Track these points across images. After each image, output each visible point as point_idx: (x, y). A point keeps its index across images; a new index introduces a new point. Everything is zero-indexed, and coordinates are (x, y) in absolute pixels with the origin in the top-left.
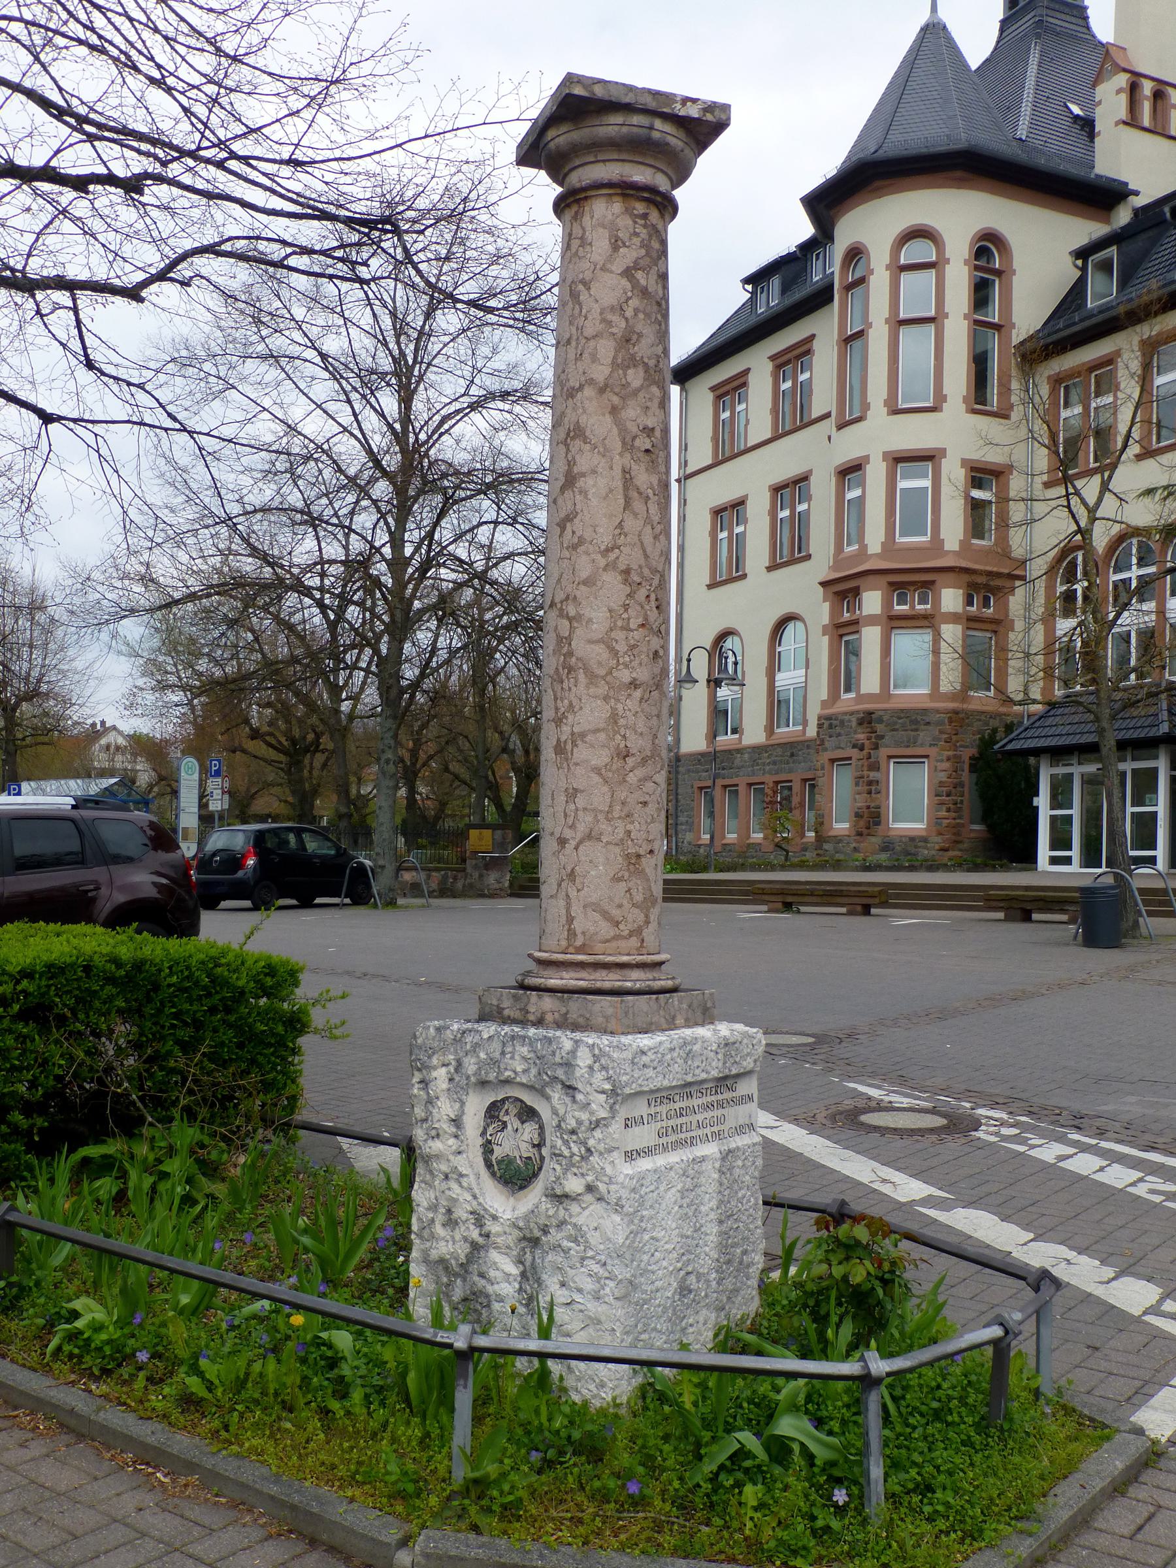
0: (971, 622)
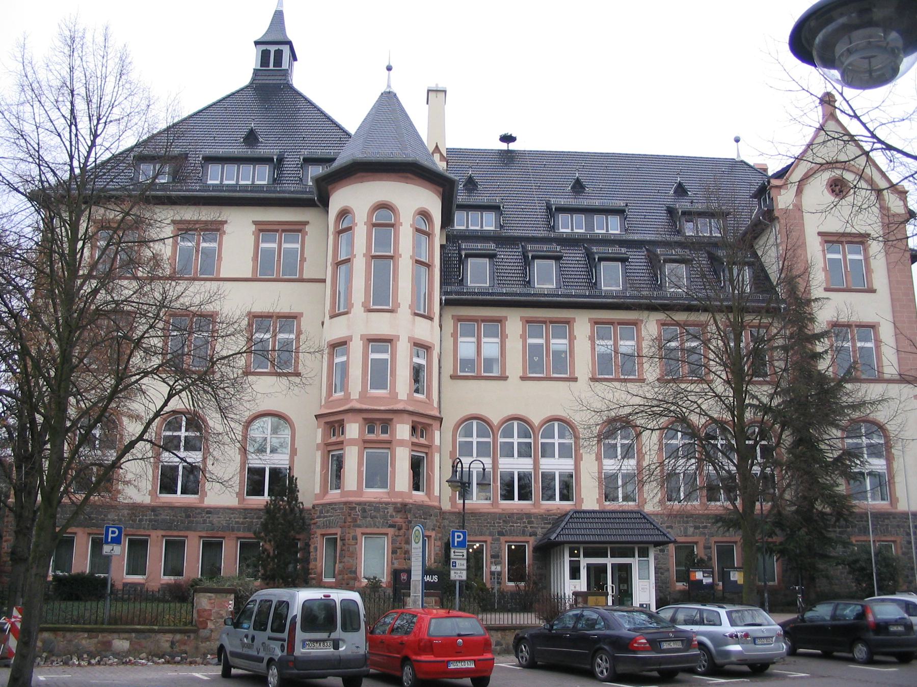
0: (366, 443)
